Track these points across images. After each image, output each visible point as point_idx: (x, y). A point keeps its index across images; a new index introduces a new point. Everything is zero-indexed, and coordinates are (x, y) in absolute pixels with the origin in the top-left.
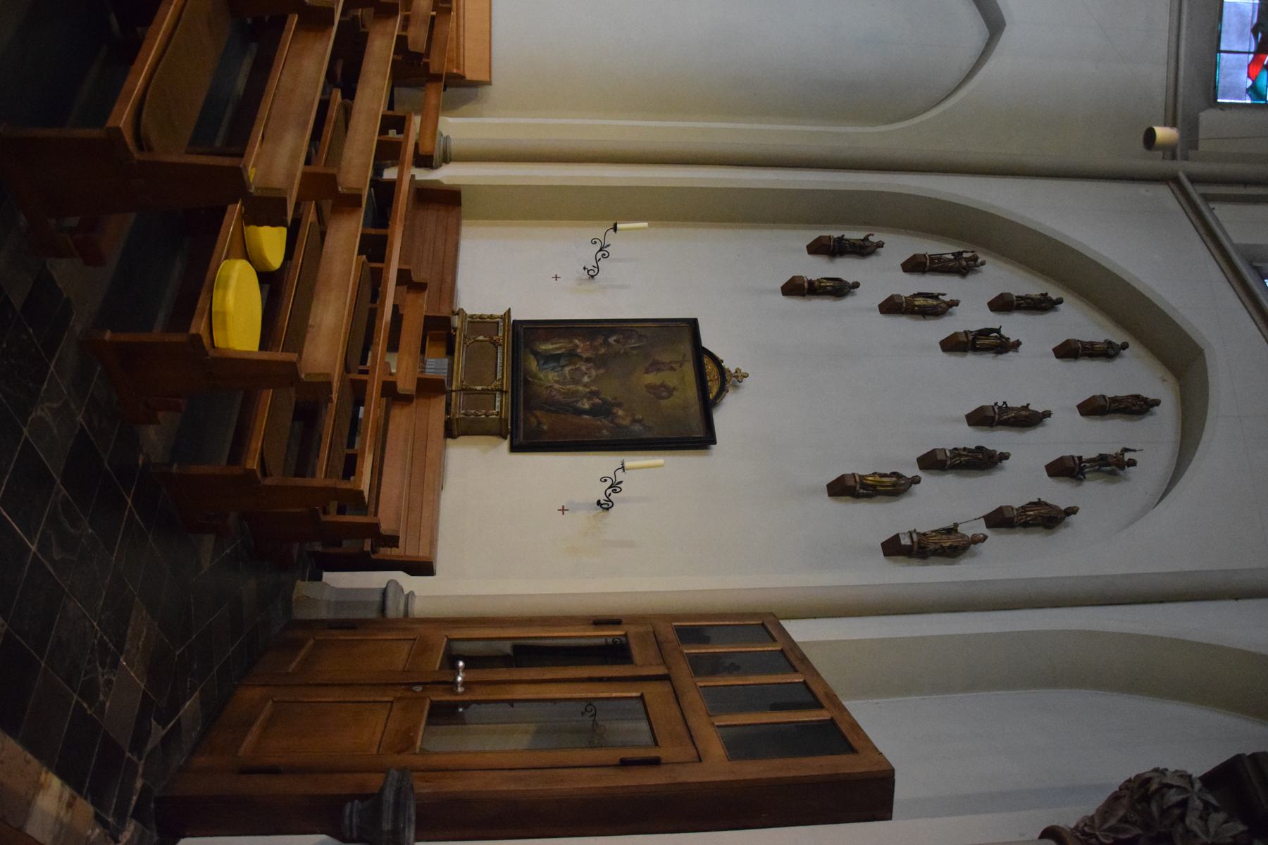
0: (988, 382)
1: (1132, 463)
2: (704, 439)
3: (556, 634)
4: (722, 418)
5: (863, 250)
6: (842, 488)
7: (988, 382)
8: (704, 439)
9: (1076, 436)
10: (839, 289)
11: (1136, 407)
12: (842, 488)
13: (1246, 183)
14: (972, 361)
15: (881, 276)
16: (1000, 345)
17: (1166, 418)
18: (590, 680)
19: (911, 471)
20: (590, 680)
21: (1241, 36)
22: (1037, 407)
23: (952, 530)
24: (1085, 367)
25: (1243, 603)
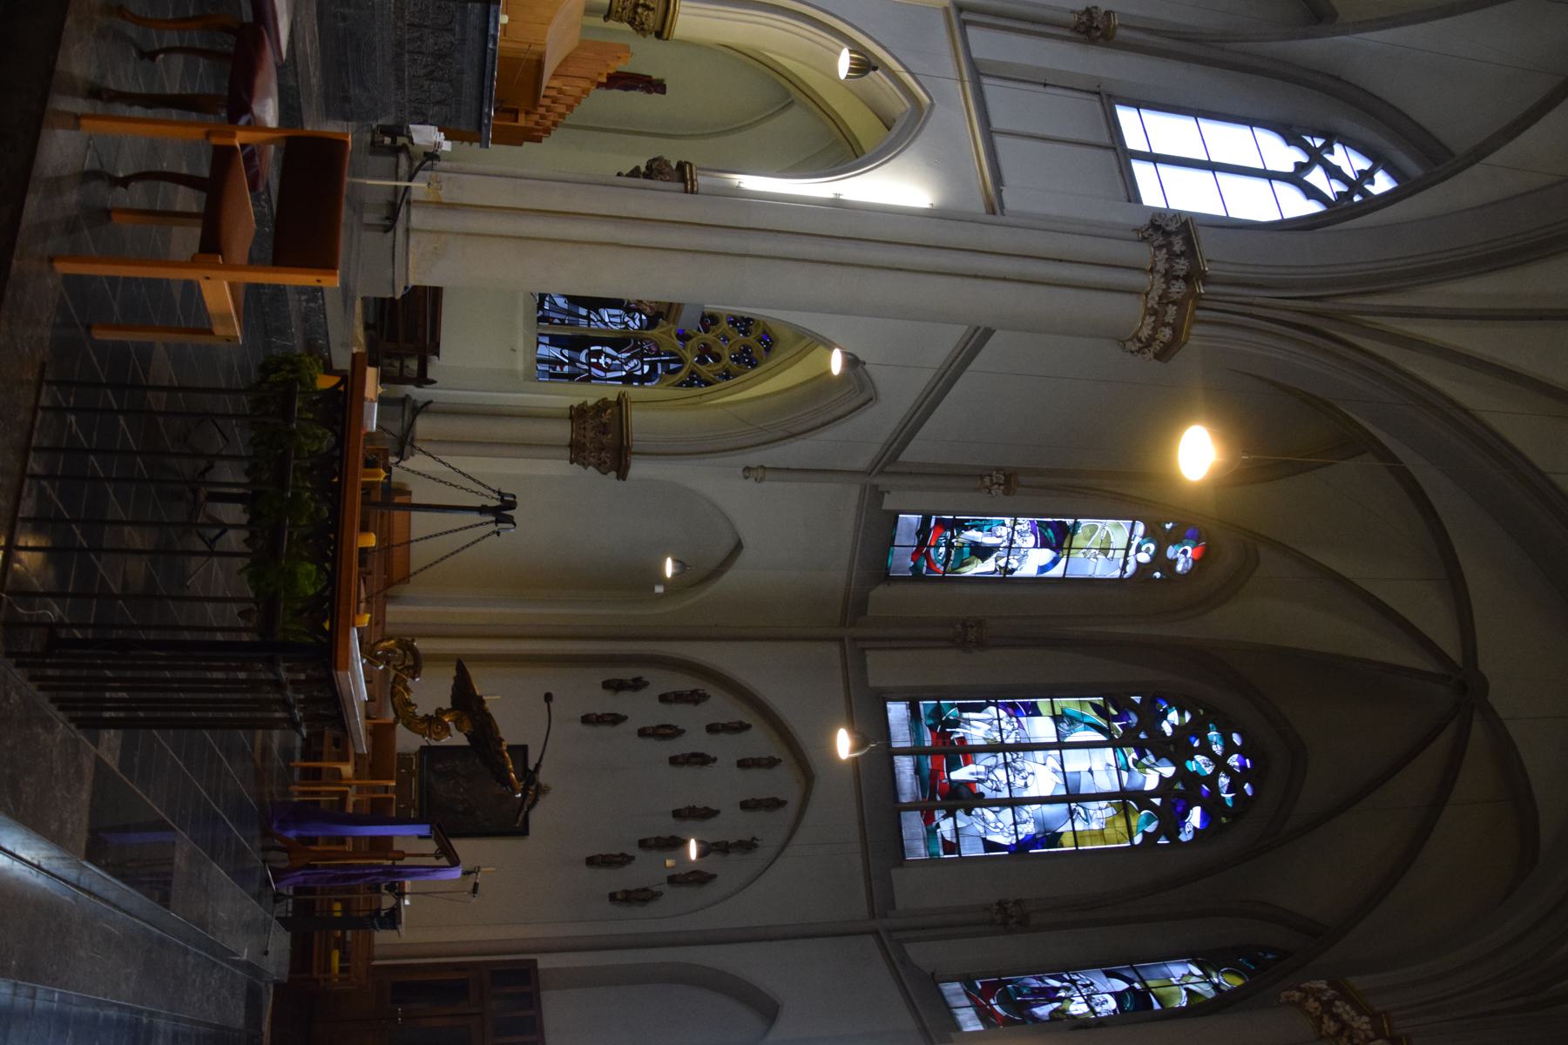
0: (692, 787)
1: (756, 846)
2: (523, 831)
3: (1340, 334)
4: (536, 817)
5: (638, 684)
6: (591, 861)
7: (692, 787)
8: (523, 831)
9: (734, 824)
10: (616, 719)
11: (775, 804)
12: (591, 861)
13: (1034, 21)
14: (688, 772)
15: (642, 709)
16: (701, 759)
17: (786, 815)
18: (1291, 339)
19: (633, 850)
20: (1291, 339)
21: (909, 537)
22: (714, 807)
23: (645, 890)
24: (755, 774)
25: (774, 943)
